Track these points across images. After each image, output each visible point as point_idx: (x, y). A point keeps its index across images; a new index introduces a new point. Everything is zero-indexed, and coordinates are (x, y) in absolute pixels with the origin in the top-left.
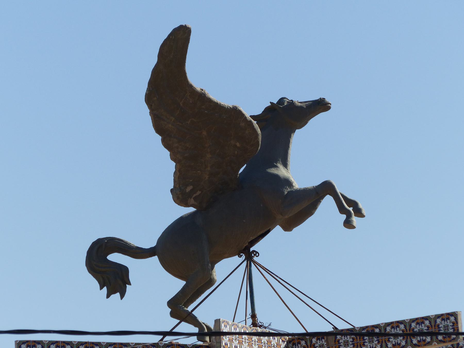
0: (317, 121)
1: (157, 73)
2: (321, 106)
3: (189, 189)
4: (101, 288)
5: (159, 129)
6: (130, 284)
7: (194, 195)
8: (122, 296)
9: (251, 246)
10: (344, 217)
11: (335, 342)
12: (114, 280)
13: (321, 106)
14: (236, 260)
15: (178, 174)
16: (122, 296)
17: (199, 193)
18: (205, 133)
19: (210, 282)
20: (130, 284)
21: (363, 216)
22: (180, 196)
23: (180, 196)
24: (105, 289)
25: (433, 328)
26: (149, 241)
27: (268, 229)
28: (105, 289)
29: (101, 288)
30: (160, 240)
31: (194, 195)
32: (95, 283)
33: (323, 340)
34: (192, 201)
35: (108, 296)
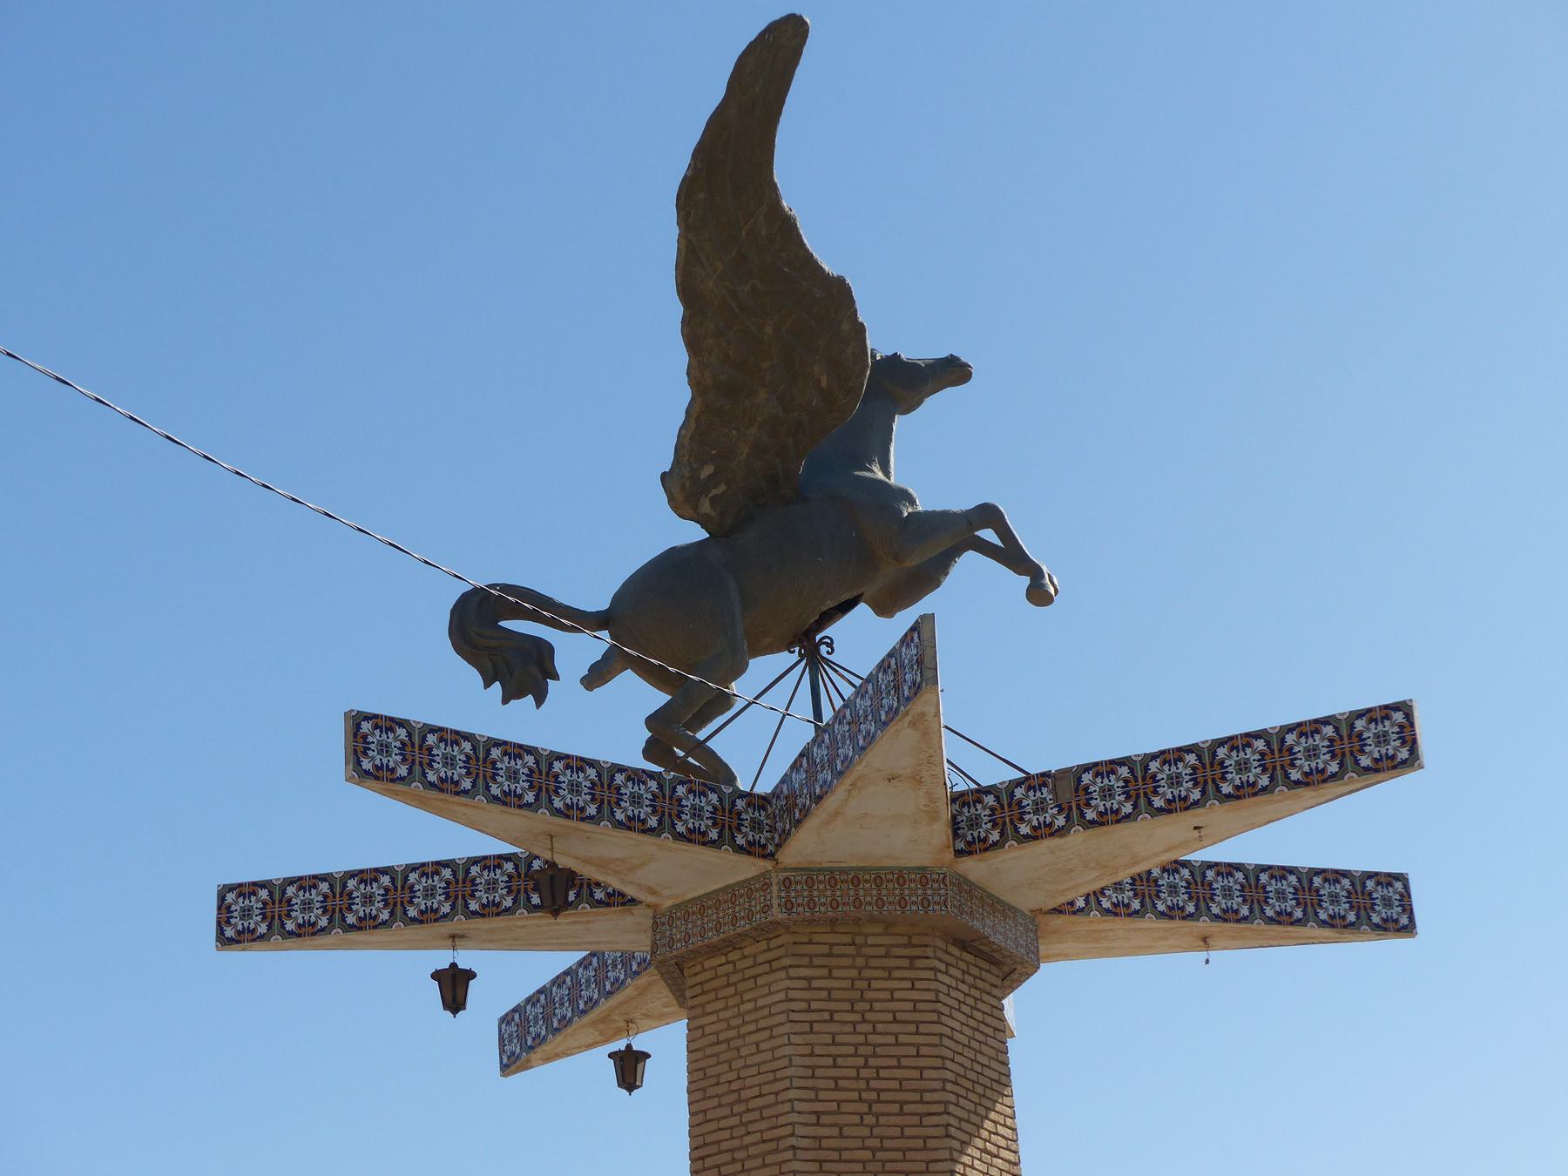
0: (940, 404)
1: (717, 125)
2: (952, 371)
3: (707, 471)
4: (487, 684)
5: (687, 289)
6: (556, 677)
7: (714, 492)
8: (539, 701)
9: (820, 630)
10: (1025, 581)
11: (1077, 790)
12: (523, 672)
13: (952, 371)
14: (785, 659)
15: (693, 426)
16: (539, 701)
17: (722, 488)
18: (769, 330)
19: (724, 701)
20: (556, 677)
21: (510, 1065)
22: (683, 489)
23: (688, 483)
24: (497, 686)
25: (1347, 750)
26: (598, 600)
27: (855, 594)
28: (497, 686)
29: (487, 684)
30: (617, 599)
31: (714, 492)
32: (473, 676)
33: (1045, 790)
34: (705, 506)
35: (505, 701)
